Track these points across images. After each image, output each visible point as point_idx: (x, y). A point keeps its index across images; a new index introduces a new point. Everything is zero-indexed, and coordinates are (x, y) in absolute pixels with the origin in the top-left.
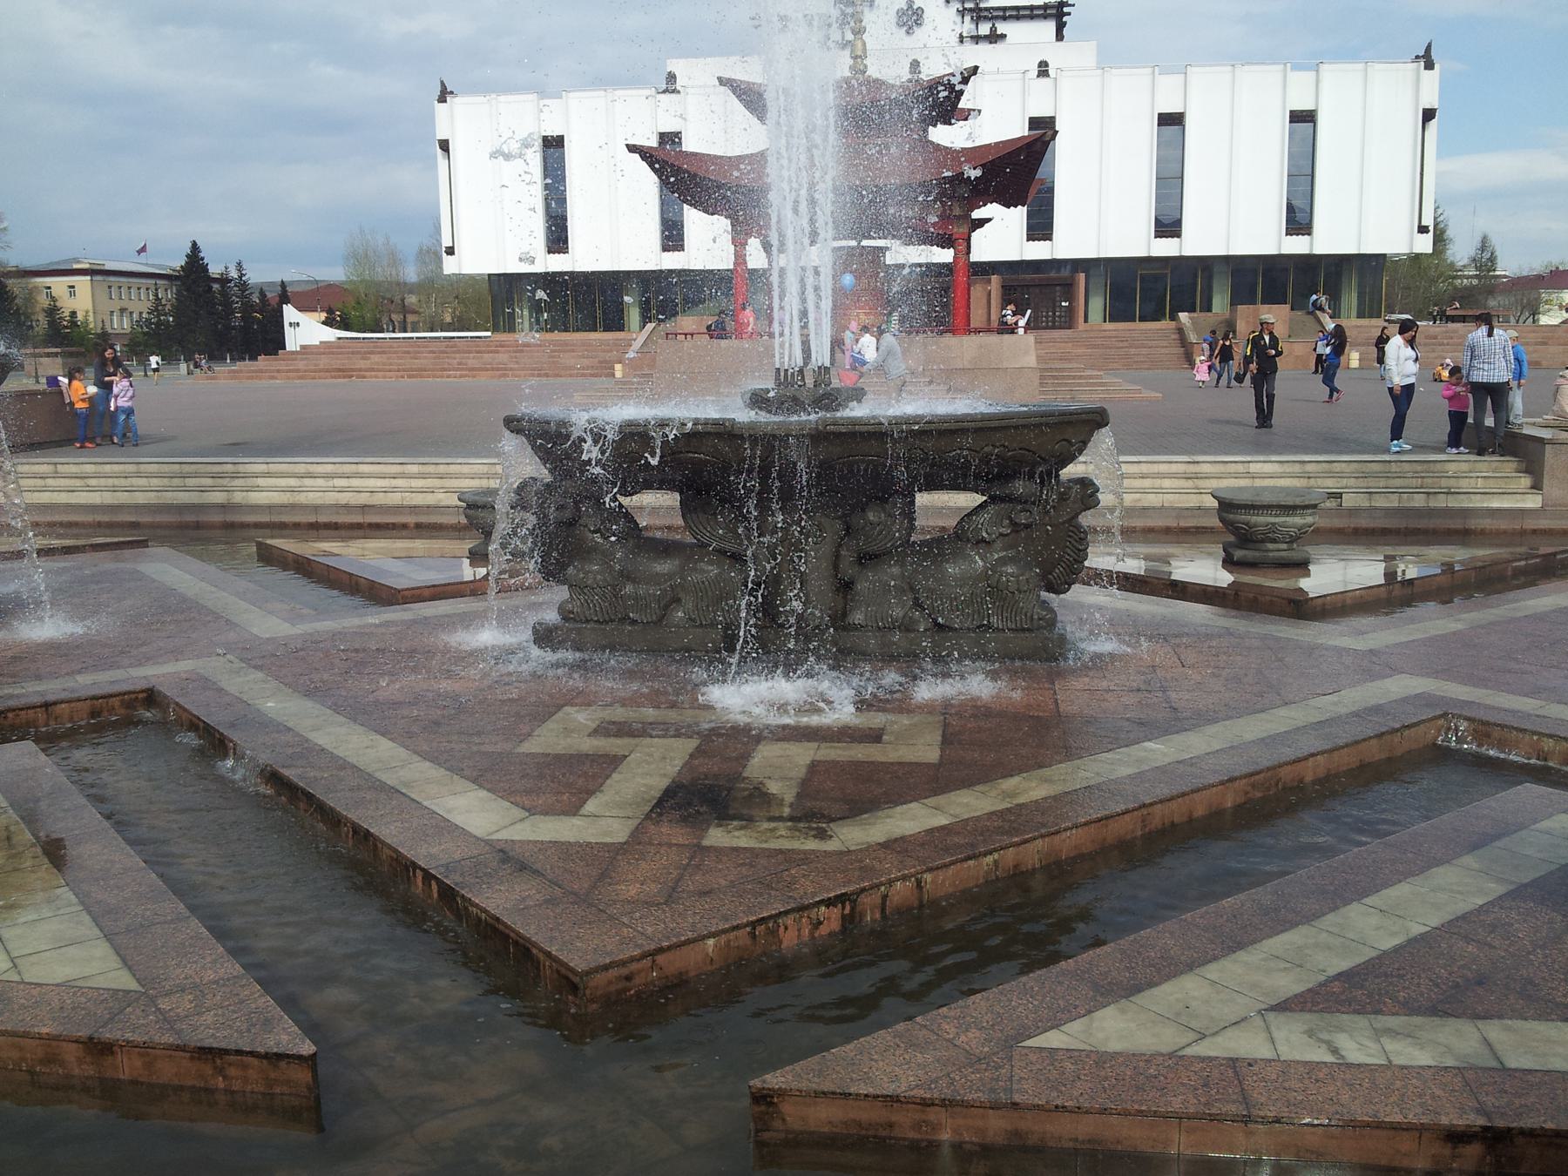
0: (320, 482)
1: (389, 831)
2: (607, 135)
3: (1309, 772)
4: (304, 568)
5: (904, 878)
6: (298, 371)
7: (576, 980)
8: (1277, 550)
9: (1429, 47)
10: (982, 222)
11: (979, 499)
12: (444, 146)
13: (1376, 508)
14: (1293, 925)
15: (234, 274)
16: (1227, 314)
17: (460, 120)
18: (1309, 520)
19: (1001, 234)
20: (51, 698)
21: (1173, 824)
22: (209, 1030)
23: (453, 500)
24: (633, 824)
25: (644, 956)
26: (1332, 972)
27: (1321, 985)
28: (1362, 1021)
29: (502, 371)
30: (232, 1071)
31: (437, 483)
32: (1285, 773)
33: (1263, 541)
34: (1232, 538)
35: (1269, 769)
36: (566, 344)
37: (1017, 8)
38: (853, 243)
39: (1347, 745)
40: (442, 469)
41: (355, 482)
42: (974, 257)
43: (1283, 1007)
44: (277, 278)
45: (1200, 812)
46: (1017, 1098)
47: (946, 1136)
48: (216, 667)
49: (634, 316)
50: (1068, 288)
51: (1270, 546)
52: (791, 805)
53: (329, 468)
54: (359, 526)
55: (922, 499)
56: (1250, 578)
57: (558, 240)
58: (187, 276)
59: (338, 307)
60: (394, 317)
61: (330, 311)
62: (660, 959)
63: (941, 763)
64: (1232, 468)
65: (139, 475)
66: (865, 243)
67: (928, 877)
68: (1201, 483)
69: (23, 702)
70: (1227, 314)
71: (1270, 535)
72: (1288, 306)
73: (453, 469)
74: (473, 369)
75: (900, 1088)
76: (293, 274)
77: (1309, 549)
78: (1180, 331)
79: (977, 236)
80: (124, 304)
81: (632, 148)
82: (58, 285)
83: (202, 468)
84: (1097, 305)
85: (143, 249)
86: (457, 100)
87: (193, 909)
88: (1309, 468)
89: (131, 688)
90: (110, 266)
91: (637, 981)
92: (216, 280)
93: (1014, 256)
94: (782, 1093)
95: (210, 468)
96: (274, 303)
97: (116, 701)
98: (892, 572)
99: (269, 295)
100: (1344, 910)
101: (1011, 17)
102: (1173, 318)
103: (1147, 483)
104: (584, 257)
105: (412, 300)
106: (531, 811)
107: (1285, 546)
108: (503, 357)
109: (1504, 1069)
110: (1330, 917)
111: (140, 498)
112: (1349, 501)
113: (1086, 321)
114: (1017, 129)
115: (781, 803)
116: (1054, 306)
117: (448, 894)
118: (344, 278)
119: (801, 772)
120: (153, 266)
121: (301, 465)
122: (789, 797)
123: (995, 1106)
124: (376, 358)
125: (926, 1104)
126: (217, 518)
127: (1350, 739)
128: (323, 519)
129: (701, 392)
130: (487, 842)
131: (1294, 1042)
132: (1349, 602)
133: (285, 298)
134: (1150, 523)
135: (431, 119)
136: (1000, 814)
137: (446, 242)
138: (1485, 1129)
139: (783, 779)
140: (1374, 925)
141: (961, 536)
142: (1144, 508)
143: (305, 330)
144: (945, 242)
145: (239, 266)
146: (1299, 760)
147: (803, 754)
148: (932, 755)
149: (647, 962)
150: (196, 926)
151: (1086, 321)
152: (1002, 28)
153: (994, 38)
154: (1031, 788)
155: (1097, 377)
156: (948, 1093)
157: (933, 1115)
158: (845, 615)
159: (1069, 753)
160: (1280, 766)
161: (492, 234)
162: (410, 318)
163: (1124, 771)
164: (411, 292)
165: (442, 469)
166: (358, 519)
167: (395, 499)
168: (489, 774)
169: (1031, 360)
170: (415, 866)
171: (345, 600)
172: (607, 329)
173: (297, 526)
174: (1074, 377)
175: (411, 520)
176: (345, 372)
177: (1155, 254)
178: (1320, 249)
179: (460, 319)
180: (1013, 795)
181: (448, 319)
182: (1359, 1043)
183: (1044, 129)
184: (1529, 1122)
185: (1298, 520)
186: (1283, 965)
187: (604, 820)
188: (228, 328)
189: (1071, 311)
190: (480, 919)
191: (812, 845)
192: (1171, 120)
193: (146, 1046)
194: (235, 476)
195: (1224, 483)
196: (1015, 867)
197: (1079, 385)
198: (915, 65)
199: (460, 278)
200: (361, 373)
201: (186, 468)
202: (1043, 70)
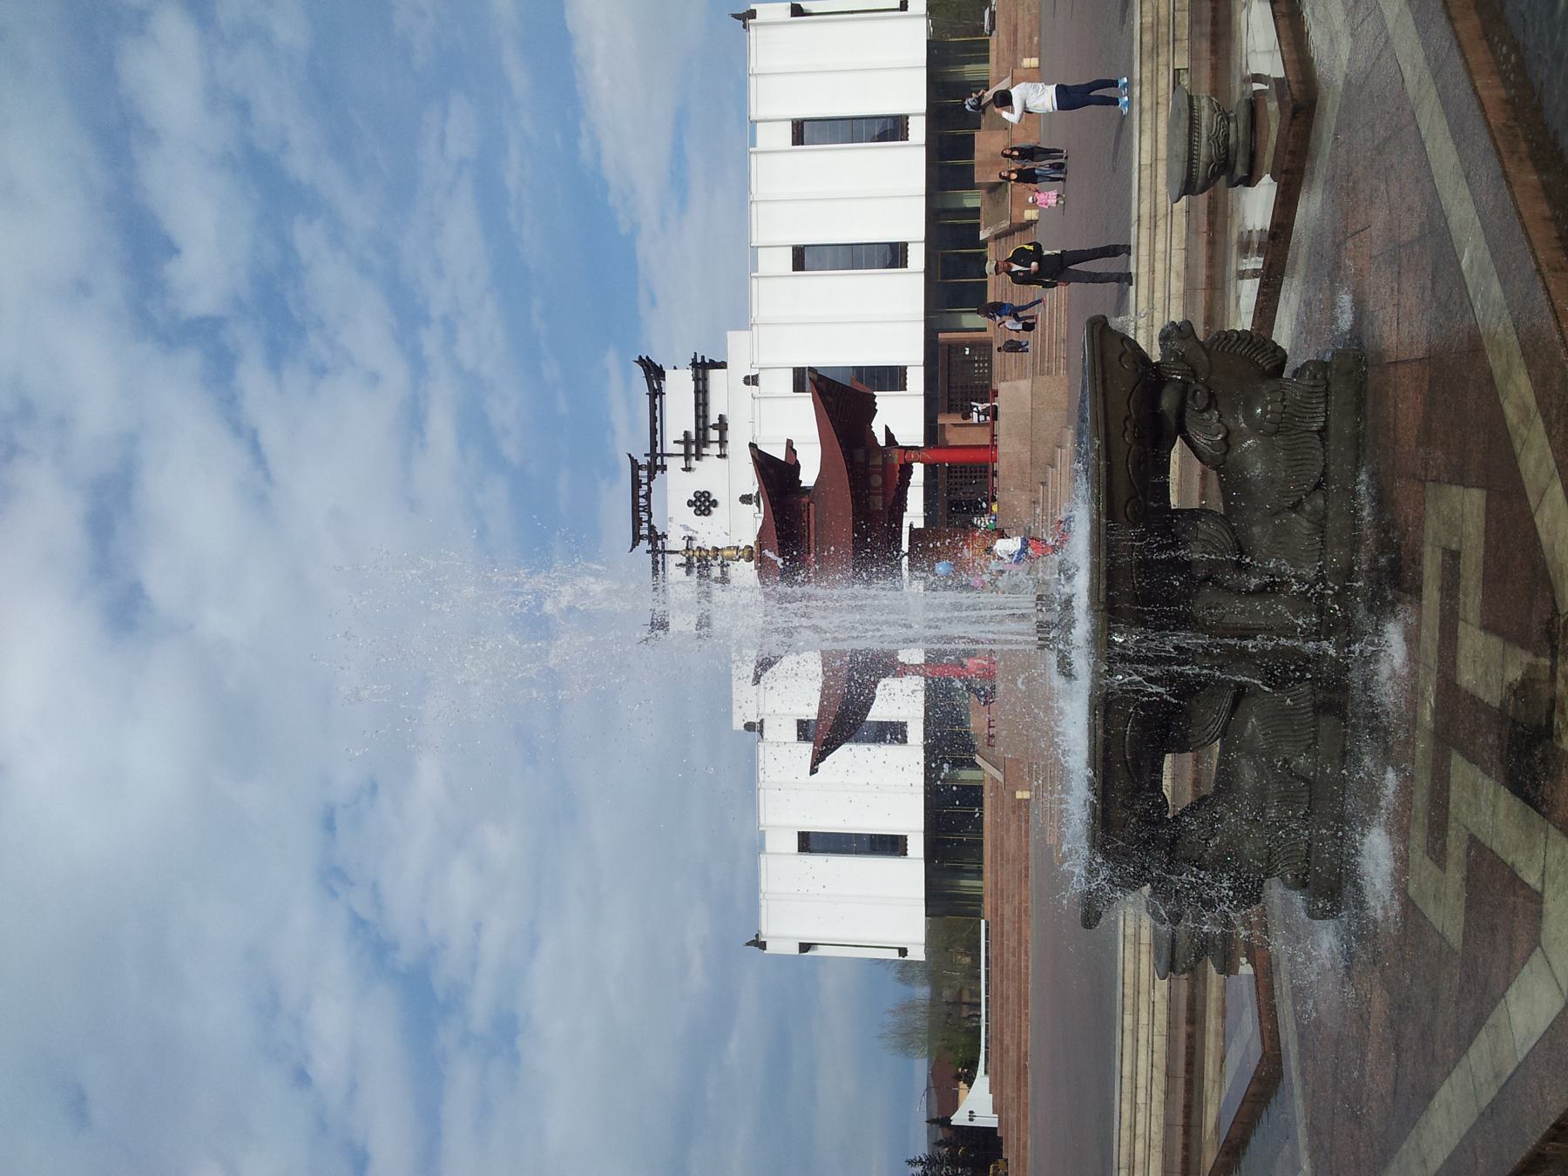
0: (1140, 1117)
2: (800, 791)
3: (1493, 92)
8: (1237, 132)
9: (736, 16)
10: (889, 436)
12: (805, 947)
13: (1190, 33)
16: (983, 192)
17: (783, 929)
18: (1204, 102)
19: (900, 417)
21: (1560, 238)
24: (1553, 831)
29: (1021, 912)
31: (1143, 998)
32: (1497, 119)
33: (1227, 148)
34: (1223, 178)
36: (995, 847)
37: (697, 405)
38: (905, 560)
39: (1463, 55)
40: (1129, 991)
41: (1141, 1081)
44: (925, 1126)
45: (1544, 209)
49: (966, 775)
50: (954, 348)
51: (1232, 140)
52: (1537, 655)
53: (1126, 1106)
54: (1189, 1085)
55: (1174, 501)
56: (1267, 159)
57: (892, 845)
59: (952, 1072)
60: (965, 1014)
61: (958, 1078)
63: (1486, 486)
64: (1146, 182)
68: (1161, 211)
70: (983, 192)
72: (977, 134)
73: (1129, 980)
74: (1020, 944)
76: (920, 1112)
78: (997, 237)
79: (902, 441)
81: (813, 771)
86: (764, 931)
96: (949, 1133)
99: (941, 1137)
102: (984, 244)
103: (1159, 266)
104: (909, 820)
105: (947, 994)
107: (1232, 125)
108: (1008, 910)
112: (1182, 61)
113: (984, 330)
114: (805, 404)
115: (1532, 668)
116: (969, 361)
118: (926, 1060)
119: (1495, 642)
122: (1527, 657)
124: (1007, 1039)
127: (1456, 52)
128: (1180, 1119)
132: (1294, 56)
133: (944, 1122)
135: (781, 959)
137: (894, 955)
139: (1503, 667)
141: (1221, 463)
142: (1187, 268)
143: (977, 1105)
144: (907, 471)
145: (911, 1163)
146: (1481, 105)
147: (1474, 642)
151: (984, 330)
153: (722, 426)
154: (1518, 391)
159: (1475, 347)
160: (1488, 124)
161: (887, 909)
162: (966, 998)
163: (1496, 290)
164: (940, 994)
165: (1129, 991)
166: (1180, 1084)
167: (1160, 1043)
169: (1024, 385)
173: (1186, 1147)
174: (1043, 341)
175: (1183, 1030)
176: (1021, 1072)
178: (922, 106)
180: (1525, 409)
181: (968, 960)
183: (803, 379)
185: (1205, 114)
189: (973, 345)
195: (1162, 187)
197: (1050, 336)
198: (746, 499)
199: (928, 944)
200: (1022, 1057)
202: (752, 380)
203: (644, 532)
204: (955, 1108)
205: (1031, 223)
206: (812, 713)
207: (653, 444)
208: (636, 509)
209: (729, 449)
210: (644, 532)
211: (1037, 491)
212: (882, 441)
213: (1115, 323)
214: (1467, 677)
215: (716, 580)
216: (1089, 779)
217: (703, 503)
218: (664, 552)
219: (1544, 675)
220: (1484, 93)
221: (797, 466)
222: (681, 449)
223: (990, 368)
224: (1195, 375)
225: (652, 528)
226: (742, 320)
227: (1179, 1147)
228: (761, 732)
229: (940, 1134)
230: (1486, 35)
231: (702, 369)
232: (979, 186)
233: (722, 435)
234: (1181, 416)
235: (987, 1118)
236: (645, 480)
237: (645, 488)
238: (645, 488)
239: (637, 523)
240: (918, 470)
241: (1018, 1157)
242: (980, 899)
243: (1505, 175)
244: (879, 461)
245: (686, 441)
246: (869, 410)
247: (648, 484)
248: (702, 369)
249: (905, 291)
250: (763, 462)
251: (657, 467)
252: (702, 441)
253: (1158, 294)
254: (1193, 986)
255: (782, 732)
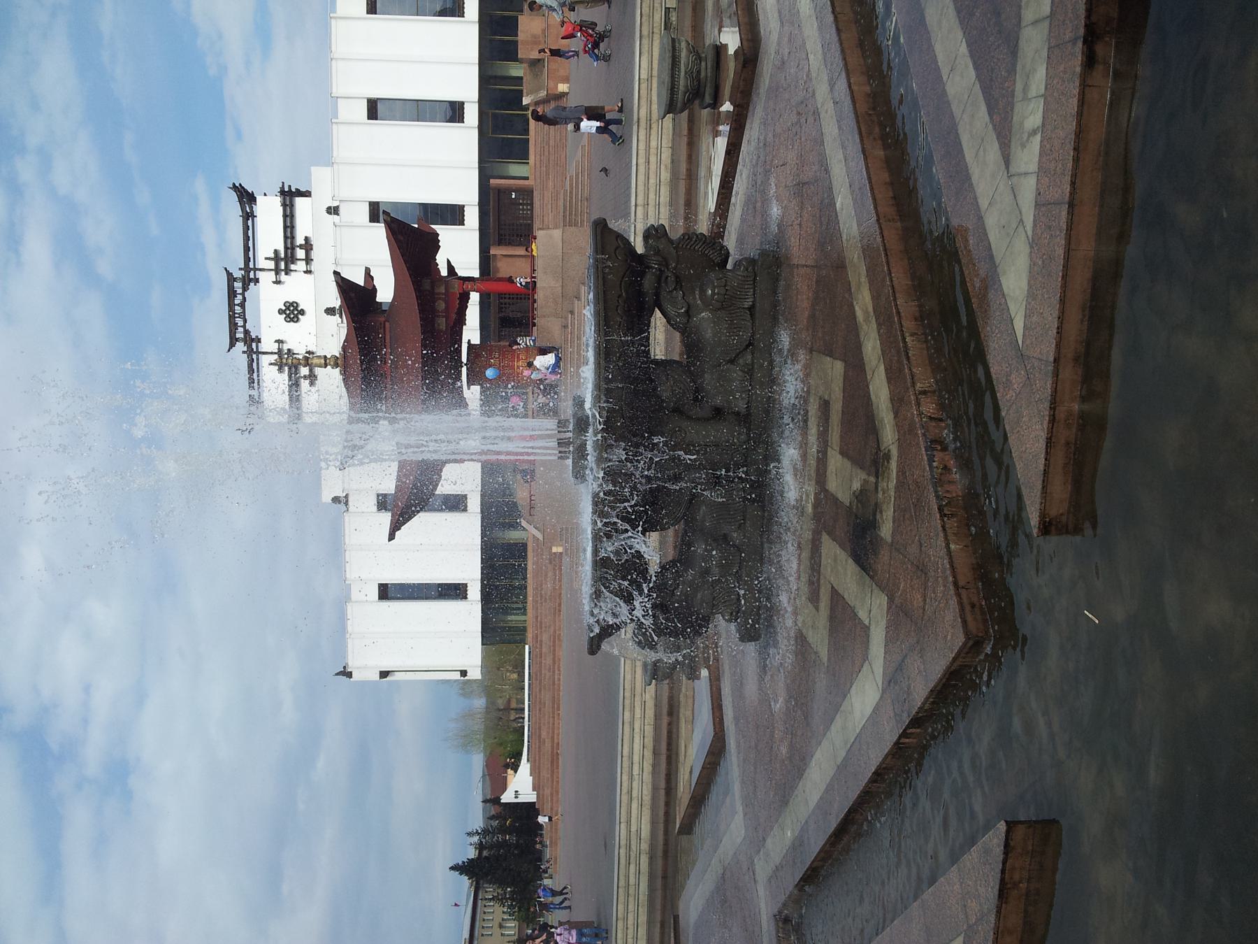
0: (635, 784)
1: (874, 757)
4: (699, 799)
5: (918, 404)
7: (971, 643)
8: (706, 69)
10: (451, 268)
11: (658, 313)
12: (384, 674)
14: (957, 136)
15: (476, 839)
17: (365, 665)
18: (683, 45)
19: (459, 250)
21: (894, 198)
22: (989, 892)
23: (652, 689)
24: (876, 590)
25: (958, 595)
26: (987, 118)
27: (995, 129)
28: (1018, 107)
29: (556, 639)
30: (1017, 877)
31: (638, 699)
33: (699, 81)
34: (697, 102)
35: (858, 122)
37: (285, 227)
38: (464, 370)
39: (844, 59)
40: (627, 694)
41: (636, 758)
42: (476, 274)
43: (1007, 160)
45: (885, 176)
46: (1052, 359)
47: (1076, 407)
48: (763, 870)
50: (502, 192)
51: (703, 74)
52: (869, 475)
54: (669, 758)
57: (455, 591)
59: (502, 761)
60: (512, 718)
61: (507, 766)
62: (961, 583)
65: (626, 919)
66: (464, 359)
67: (919, 386)
71: (695, 76)
75: (1043, 435)
77: (708, 42)
79: (461, 273)
80: (496, 925)
81: (392, 537)
84: (516, 169)
87: (916, 898)
88: (645, 33)
90: (466, 935)
91: (975, 599)
92: (480, 853)
93: (476, 236)
94: (1043, 515)
96: (499, 809)
98: (708, 380)
99: (493, 813)
100: (950, 97)
101: (292, 233)
103: (653, 159)
104: (469, 571)
105: (501, 703)
106: (865, 658)
107: (703, 64)
108: (545, 637)
109: (1053, 14)
110: (954, 107)
111: (643, 918)
113: (527, 178)
114: (380, 230)
116: (515, 203)
117: (916, 722)
119: (848, 464)
121: (621, 797)
122: (863, 476)
123: (1056, 374)
124: (544, 734)
125: (1053, 420)
126: (660, 862)
128: (663, 784)
129: (573, 508)
130: (884, 691)
131: (1028, 157)
133: (495, 801)
134: (684, 158)
135: (364, 684)
136: (879, 325)
137: (457, 676)
138: (1085, 42)
140: (960, 80)
141: (683, 325)
142: (673, 162)
143: (521, 786)
144: (465, 298)
147: (835, 461)
148: (839, 366)
149: (963, 592)
150: (928, 895)
151: (527, 178)
152: (300, 240)
153: (308, 246)
155: (571, 180)
156: (1047, 405)
157: (1061, 414)
158: (738, 414)
161: (450, 641)
162: (514, 705)
165: (627, 694)
167: (649, 730)
168: (841, 688)
169: (557, 234)
170: (897, 743)
171: (722, 770)
172: (525, 558)
173: (667, 804)
175: (665, 720)
177: (476, 123)
179: (515, 667)
180: (866, 312)
181: (515, 676)
182: (1031, 115)
184: (1082, 12)
185: (684, 54)
186: (981, 153)
187: (872, 609)
188: (517, 846)
189: (519, 190)
190: (933, 703)
191: (894, 465)
192: (374, 109)
193: (996, 933)
196: (916, 319)
198: (330, 311)
199: (484, 666)
200: (555, 746)
201: (622, 883)
202: (333, 211)
203: (240, 335)
204: (505, 789)
205: (564, 95)
206: (389, 487)
207: (247, 260)
208: (232, 318)
209: (313, 267)
210: (240, 335)
211: (566, 318)
212: (444, 273)
213: (613, 225)
214: (832, 485)
215: (305, 377)
217: (292, 312)
218: (258, 353)
219: (872, 487)
220: (855, 88)
221: (374, 290)
222: (271, 265)
223: (532, 210)
224: (667, 266)
225: (247, 332)
226: (326, 159)
227: (662, 804)
228: (346, 503)
229: (493, 810)
230: (861, 44)
231: (289, 196)
232: (521, 61)
233: (307, 254)
234: (657, 294)
235: (528, 796)
236: (240, 291)
237: (240, 297)
238: (240, 297)
239: (233, 327)
240: (475, 297)
242: (524, 630)
243: (864, 151)
244: (442, 290)
245: (276, 258)
246: (433, 243)
247: (243, 294)
248: (289, 196)
249: (463, 142)
250: (345, 286)
251: (250, 280)
252: (290, 258)
253: (652, 181)
254: (671, 689)
255: (364, 504)
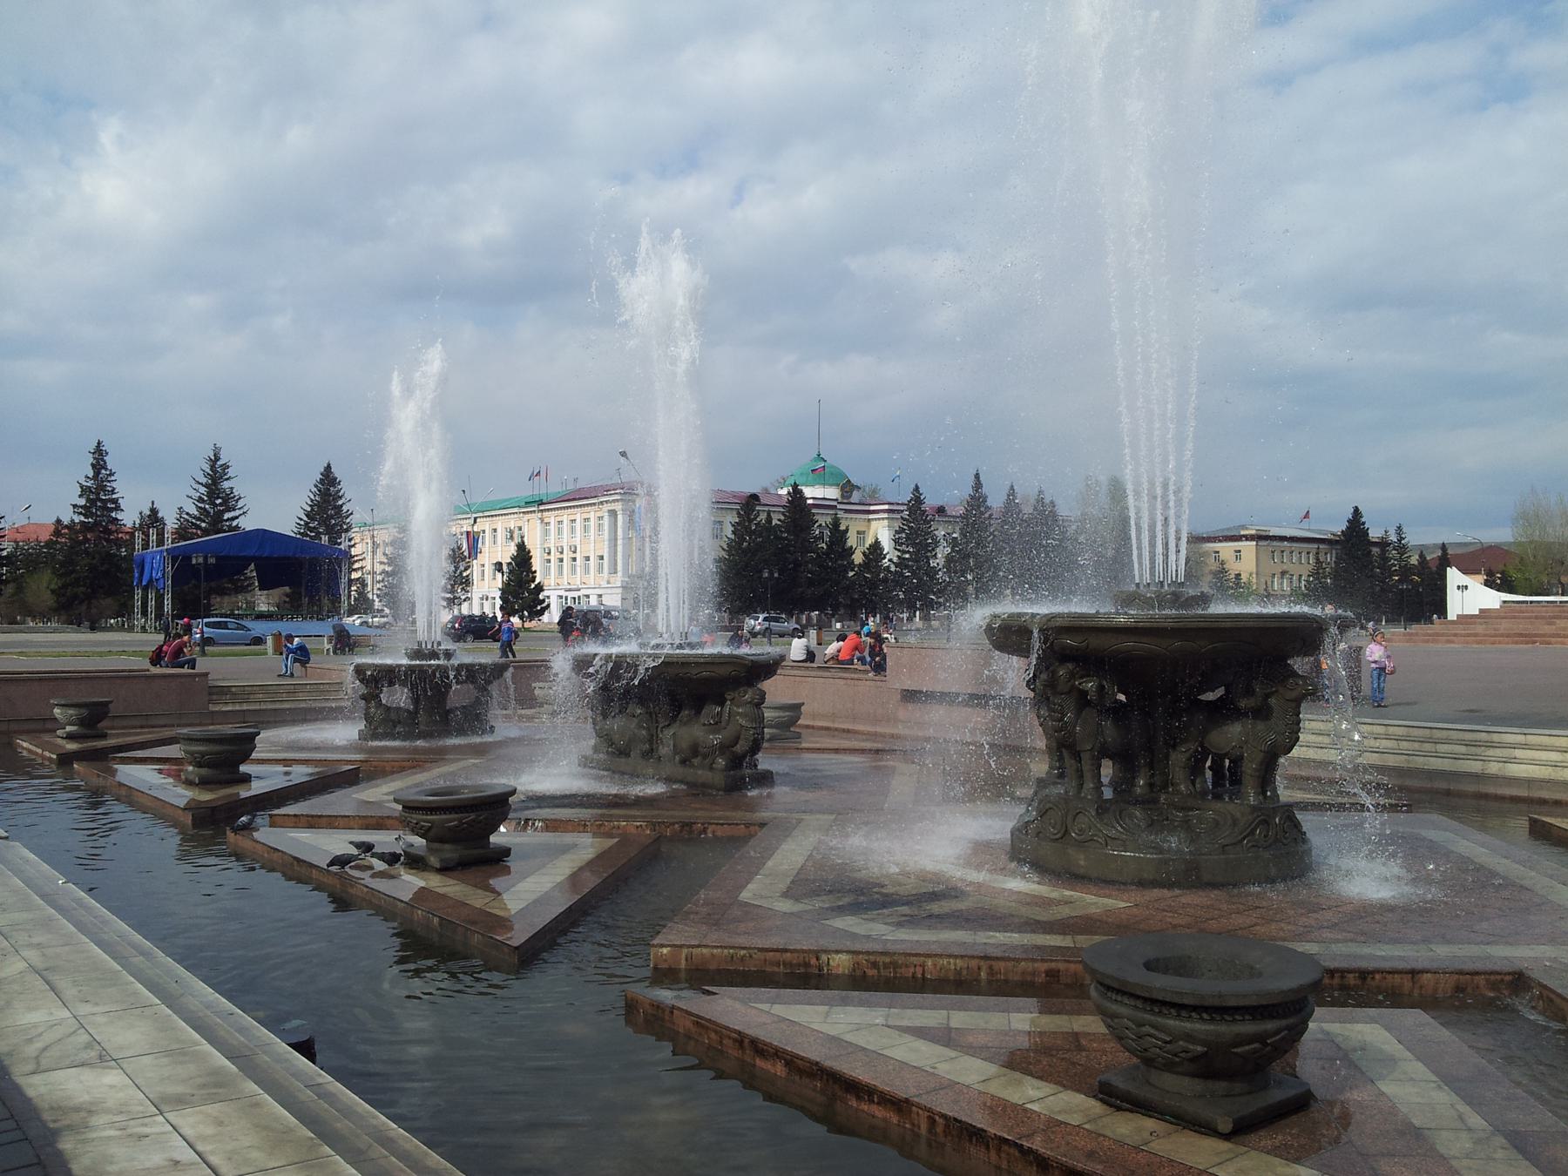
6: (1476, 635)
15: (1393, 538)
20: (1419, 966)
58: (1347, 541)
59: (1498, 569)
61: (1490, 573)
64: (1172, 557)
69: (1387, 965)
76: (1453, 536)
80: (1285, 567)
82: (1226, 549)
83: (1454, 735)
85: (1307, 516)
89: (1497, 968)
90: (1274, 531)
95: (1461, 735)
97: (1481, 980)
120: (1320, 532)
126: (1471, 788)
143: (1468, 595)
176: (1528, 638)
194: (1491, 745)
200: (1545, 639)
201: (1438, 734)
204: (1465, 571)
216: (118, 508)
227: (1500, 791)
241: (1438, 635)
